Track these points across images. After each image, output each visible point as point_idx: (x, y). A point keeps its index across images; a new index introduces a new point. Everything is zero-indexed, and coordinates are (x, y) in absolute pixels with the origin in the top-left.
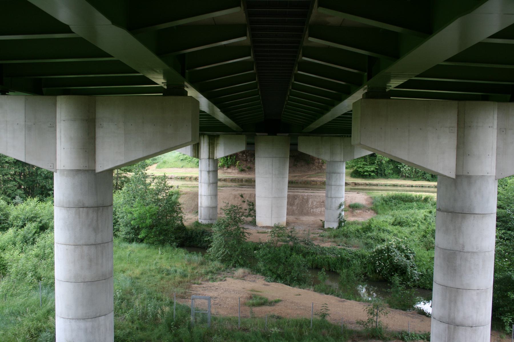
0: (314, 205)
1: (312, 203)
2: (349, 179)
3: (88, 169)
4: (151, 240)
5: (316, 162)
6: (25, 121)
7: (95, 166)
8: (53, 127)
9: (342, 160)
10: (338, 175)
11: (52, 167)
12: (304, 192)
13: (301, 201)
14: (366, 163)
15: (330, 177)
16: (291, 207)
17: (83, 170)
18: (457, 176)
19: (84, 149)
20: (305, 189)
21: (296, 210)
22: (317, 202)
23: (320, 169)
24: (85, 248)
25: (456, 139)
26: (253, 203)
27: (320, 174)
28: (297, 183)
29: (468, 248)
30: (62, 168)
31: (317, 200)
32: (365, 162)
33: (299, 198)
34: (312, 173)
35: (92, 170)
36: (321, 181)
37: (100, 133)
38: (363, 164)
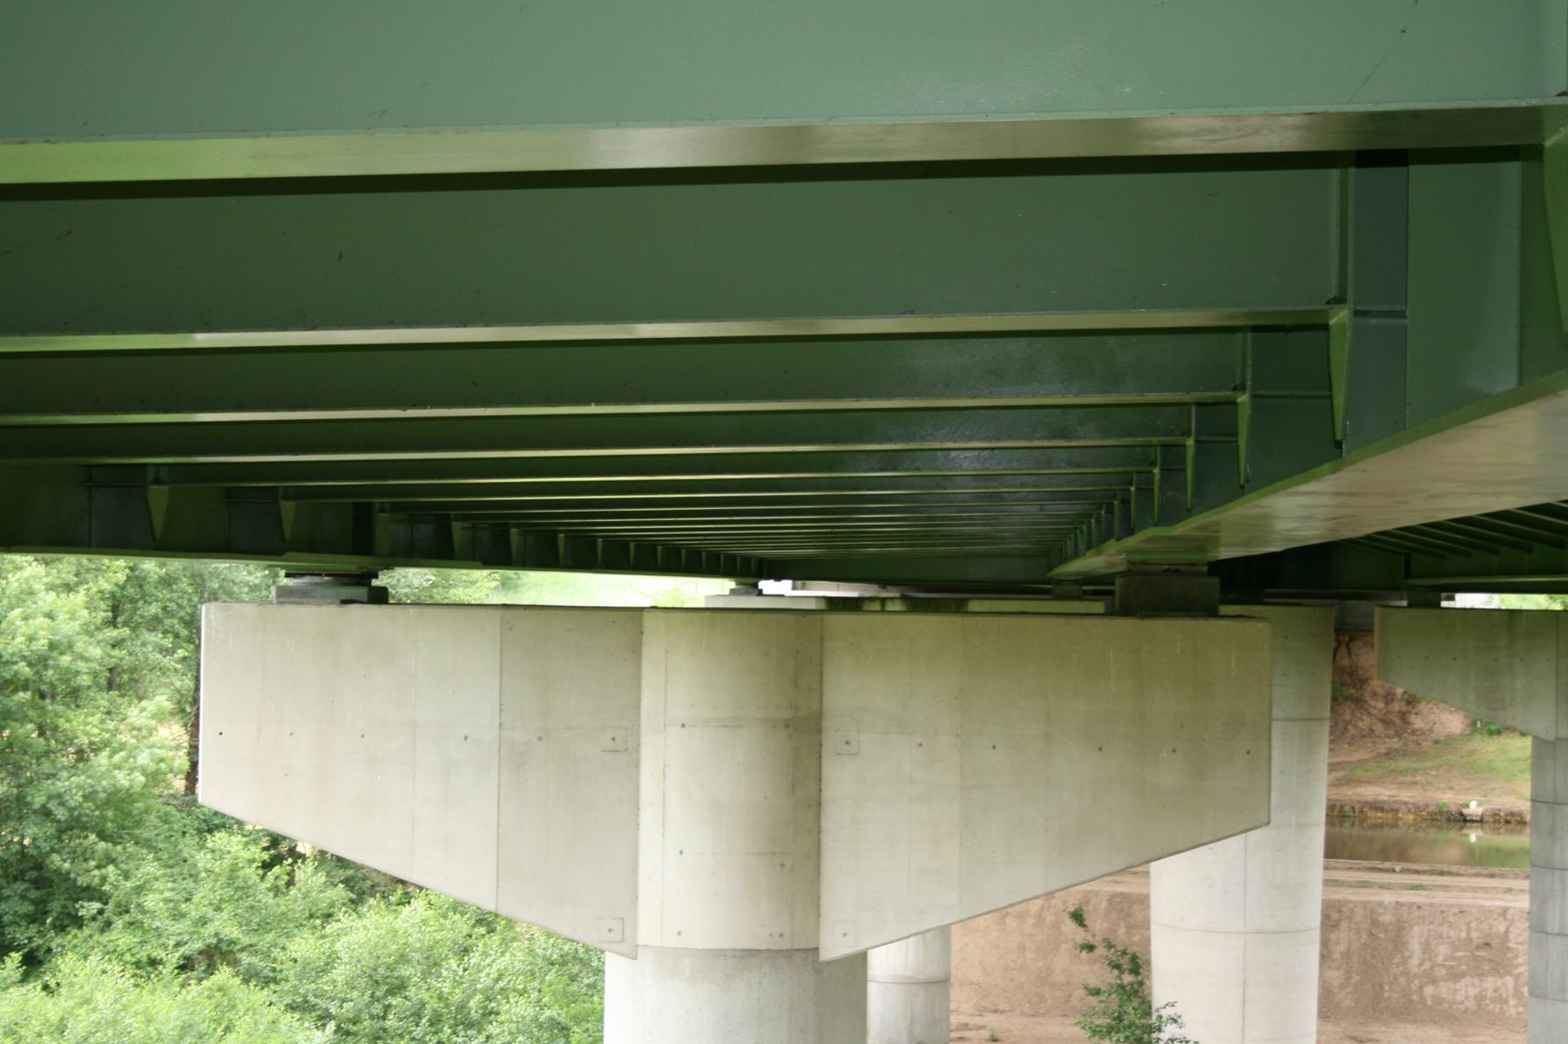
0: (1440, 959)
1: (1427, 948)
3: (789, 947)
5: (1374, 694)
6: (501, 725)
7: (817, 931)
8: (627, 750)
11: (616, 935)
12: (1365, 885)
13: (1364, 938)
15: (1553, 827)
17: (769, 950)
19: (773, 854)
20: (1365, 863)
21: (1343, 986)
22: (1454, 947)
26: (1134, 958)
27: (1403, 764)
30: (975, 974)
31: (1452, 934)
33: (1350, 918)
34: (1355, 757)
36: (1417, 809)
37: (840, 779)
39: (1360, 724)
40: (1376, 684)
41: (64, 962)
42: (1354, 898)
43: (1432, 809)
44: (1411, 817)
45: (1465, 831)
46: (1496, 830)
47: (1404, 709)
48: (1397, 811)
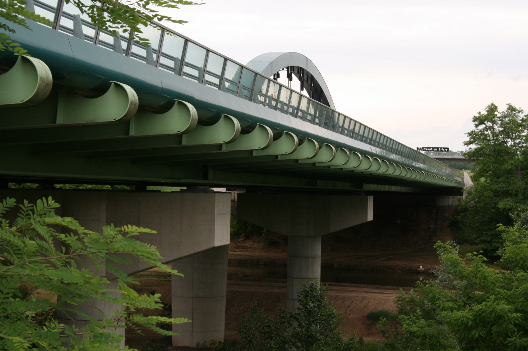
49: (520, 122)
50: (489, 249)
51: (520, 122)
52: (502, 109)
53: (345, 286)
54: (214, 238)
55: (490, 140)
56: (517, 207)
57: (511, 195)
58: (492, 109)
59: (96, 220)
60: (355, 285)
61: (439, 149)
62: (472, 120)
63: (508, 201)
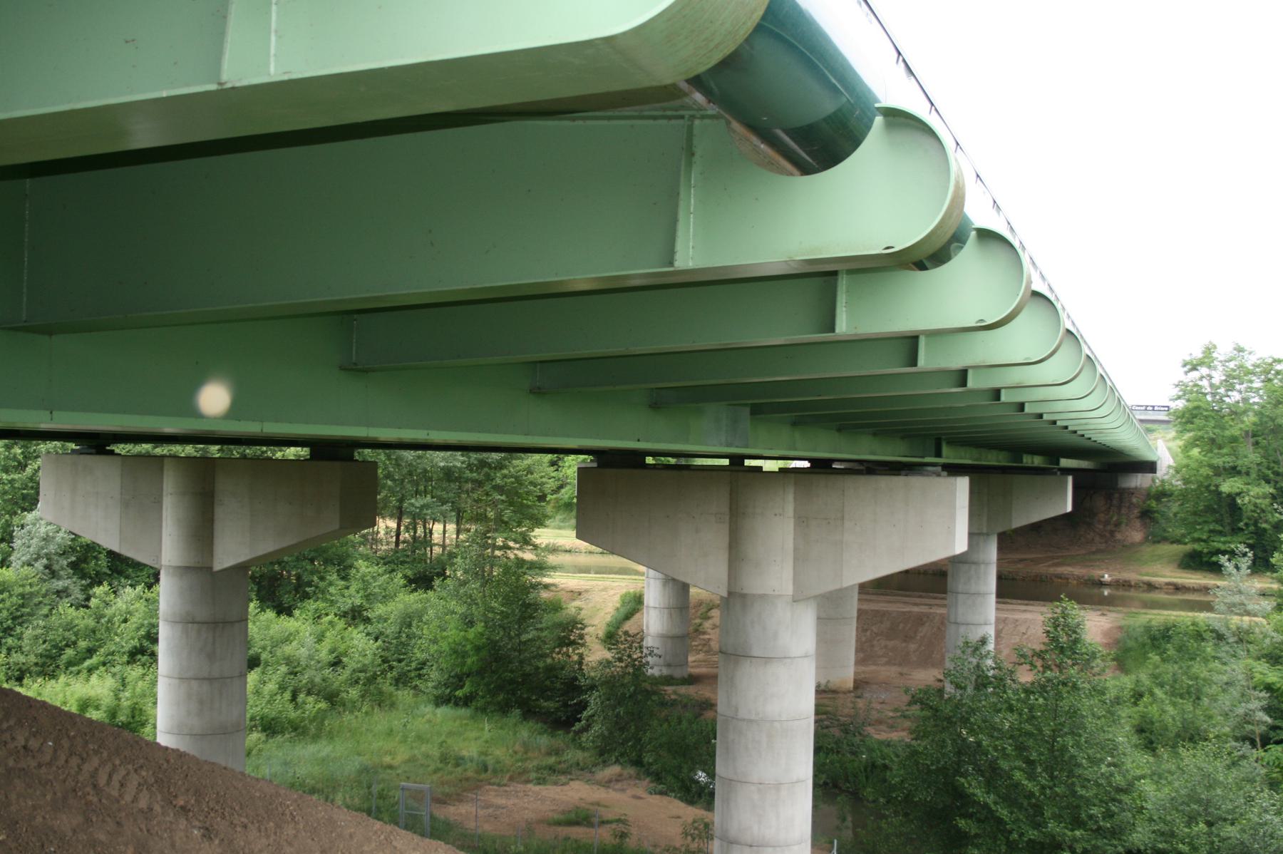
2: (1168, 574)
4: (480, 703)
8: (159, 502)
9: (985, 531)
10: (973, 567)
14: (1219, 528)
16: (904, 645)
18: (730, 593)
21: (914, 652)
23: (1106, 542)
24: (194, 684)
25: (728, 532)
28: (1013, 579)
29: (743, 713)
30: (168, 564)
32: (1217, 523)
35: (207, 568)
36: (1078, 578)
37: (220, 513)
38: (1211, 531)
39: (1088, 536)
40: (1102, 516)
41: (954, 716)
42: (938, 612)
43: (1086, 578)
44: (1075, 582)
45: (1101, 590)
46: (1117, 589)
47: (1114, 529)
48: (1068, 579)
49: (1252, 368)
50: (1205, 551)
51: (1252, 368)
52: (1223, 351)
53: (1012, 604)
54: (954, 541)
55: (1205, 394)
56: (1249, 490)
57: (1239, 473)
58: (1209, 350)
59: (780, 515)
60: (1026, 602)
61: (1156, 408)
62: (1181, 365)
63: (1235, 481)
